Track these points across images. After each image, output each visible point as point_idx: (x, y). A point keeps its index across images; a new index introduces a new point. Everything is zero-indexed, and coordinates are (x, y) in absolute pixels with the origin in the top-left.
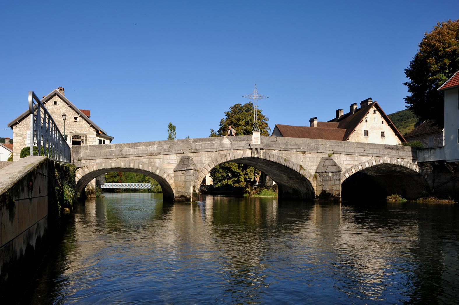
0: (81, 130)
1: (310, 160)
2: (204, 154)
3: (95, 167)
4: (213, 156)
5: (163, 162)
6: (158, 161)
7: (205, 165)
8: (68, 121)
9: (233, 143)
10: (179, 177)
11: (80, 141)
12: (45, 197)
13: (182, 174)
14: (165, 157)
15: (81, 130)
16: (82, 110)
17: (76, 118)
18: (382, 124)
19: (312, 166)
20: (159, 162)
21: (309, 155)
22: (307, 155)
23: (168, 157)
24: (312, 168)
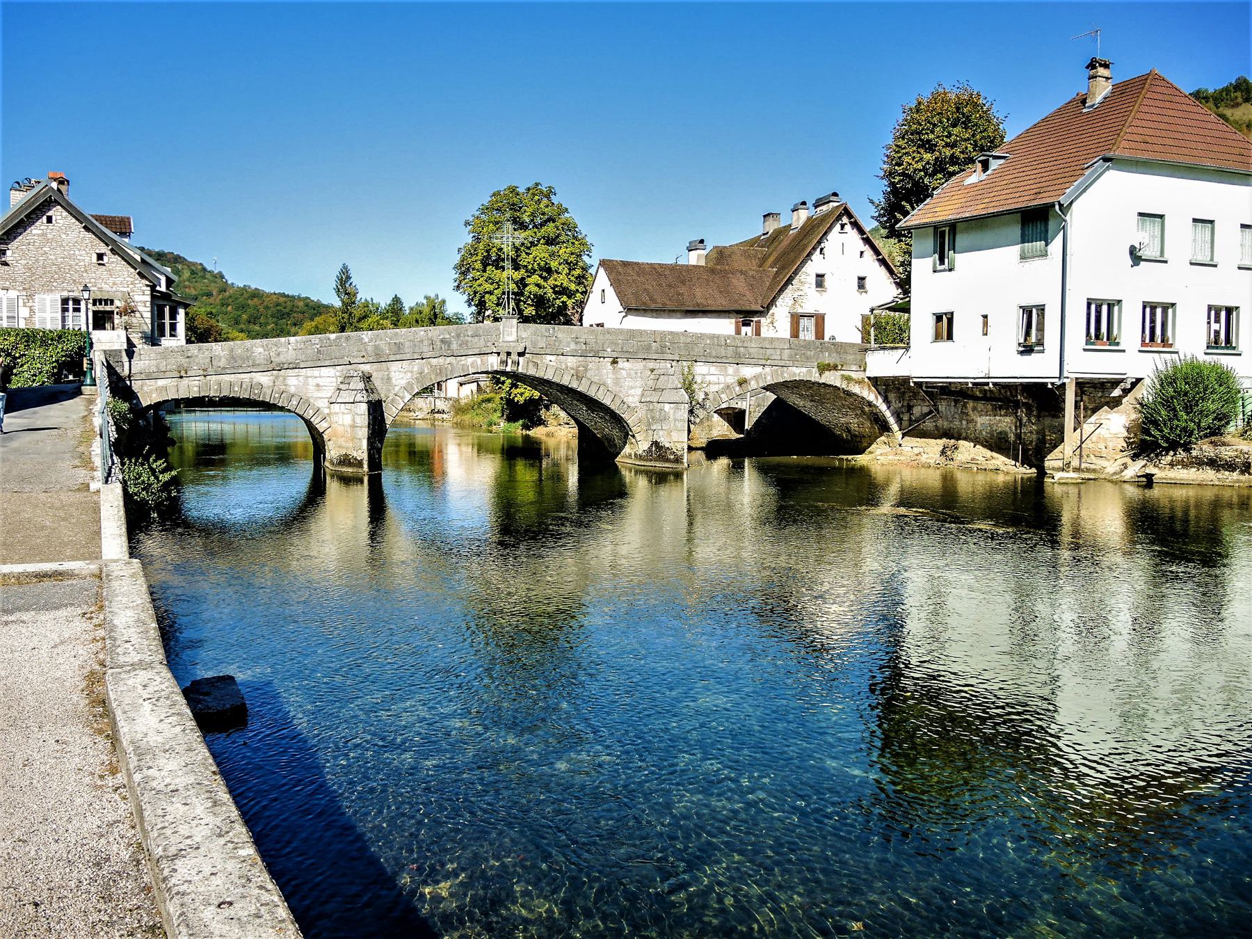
0: (114, 284)
1: (629, 375)
2: (394, 367)
3: (154, 395)
4: (416, 369)
5: (306, 384)
6: (293, 381)
7: (397, 389)
8: (82, 263)
9: (1046, 692)
10: (341, 415)
11: (112, 312)
12: (47, 583)
13: (346, 411)
14: (309, 372)
15: (114, 284)
16: (98, 218)
17: (100, 257)
18: (944, 345)
19: (632, 388)
20: (296, 383)
21: (627, 365)
22: (622, 364)
23: (316, 372)
24: (632, 392)
